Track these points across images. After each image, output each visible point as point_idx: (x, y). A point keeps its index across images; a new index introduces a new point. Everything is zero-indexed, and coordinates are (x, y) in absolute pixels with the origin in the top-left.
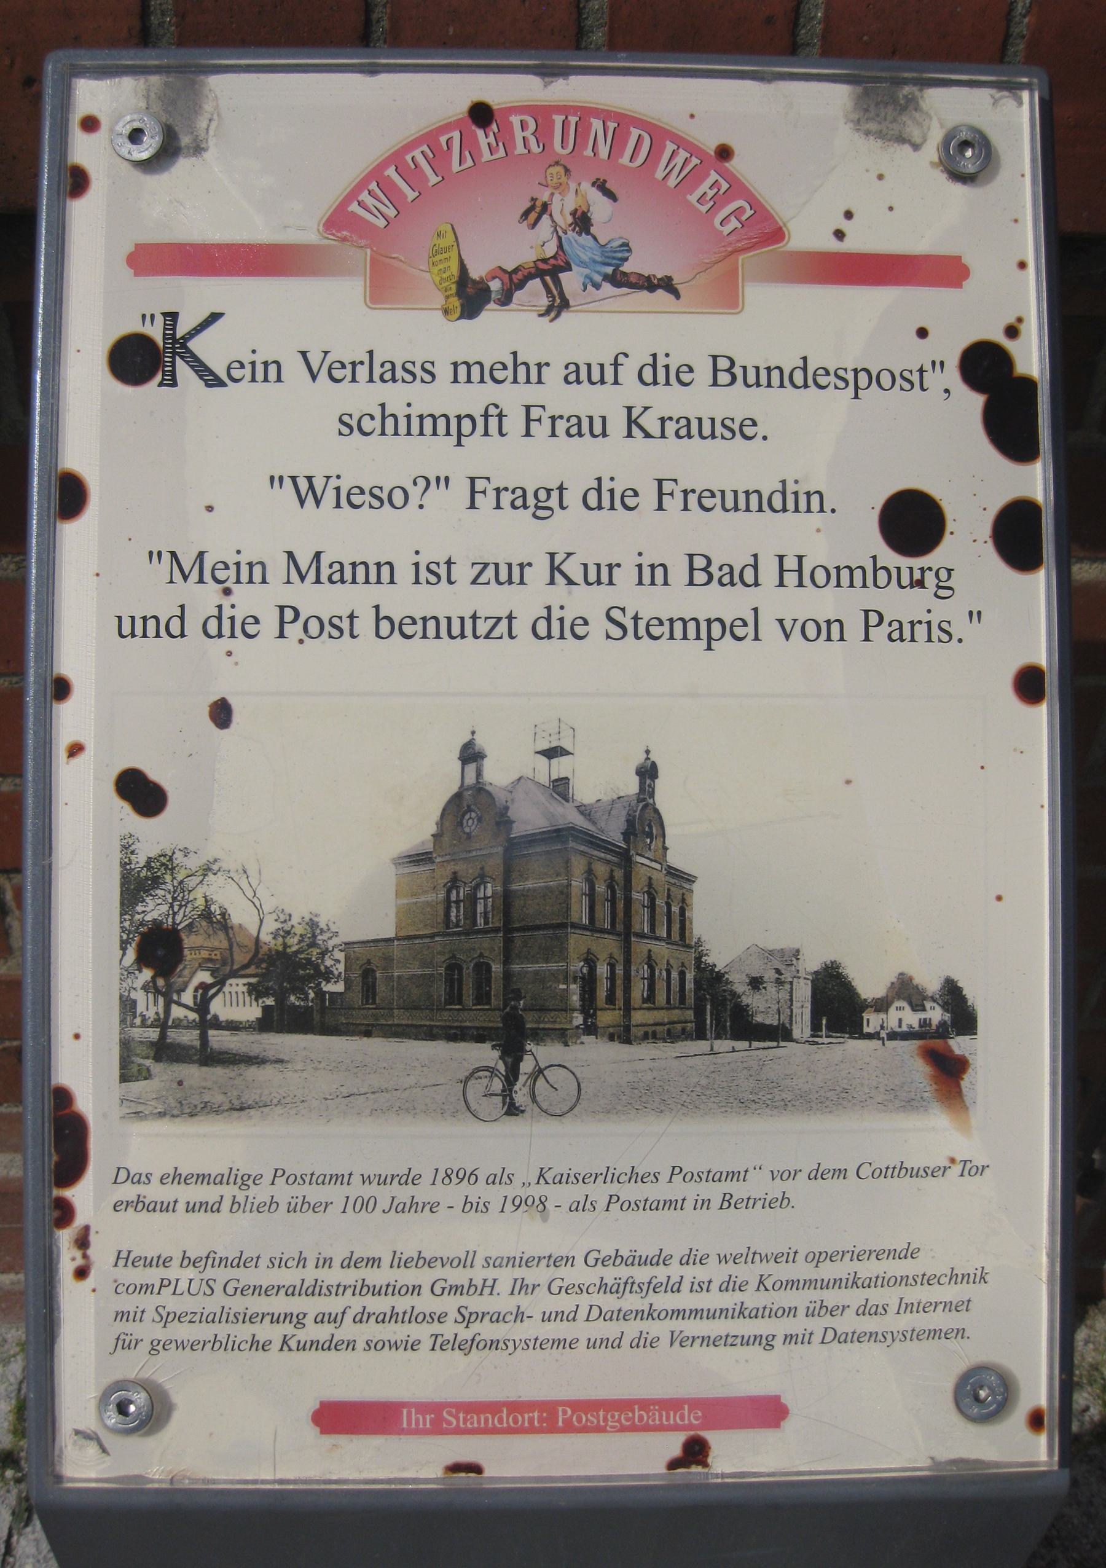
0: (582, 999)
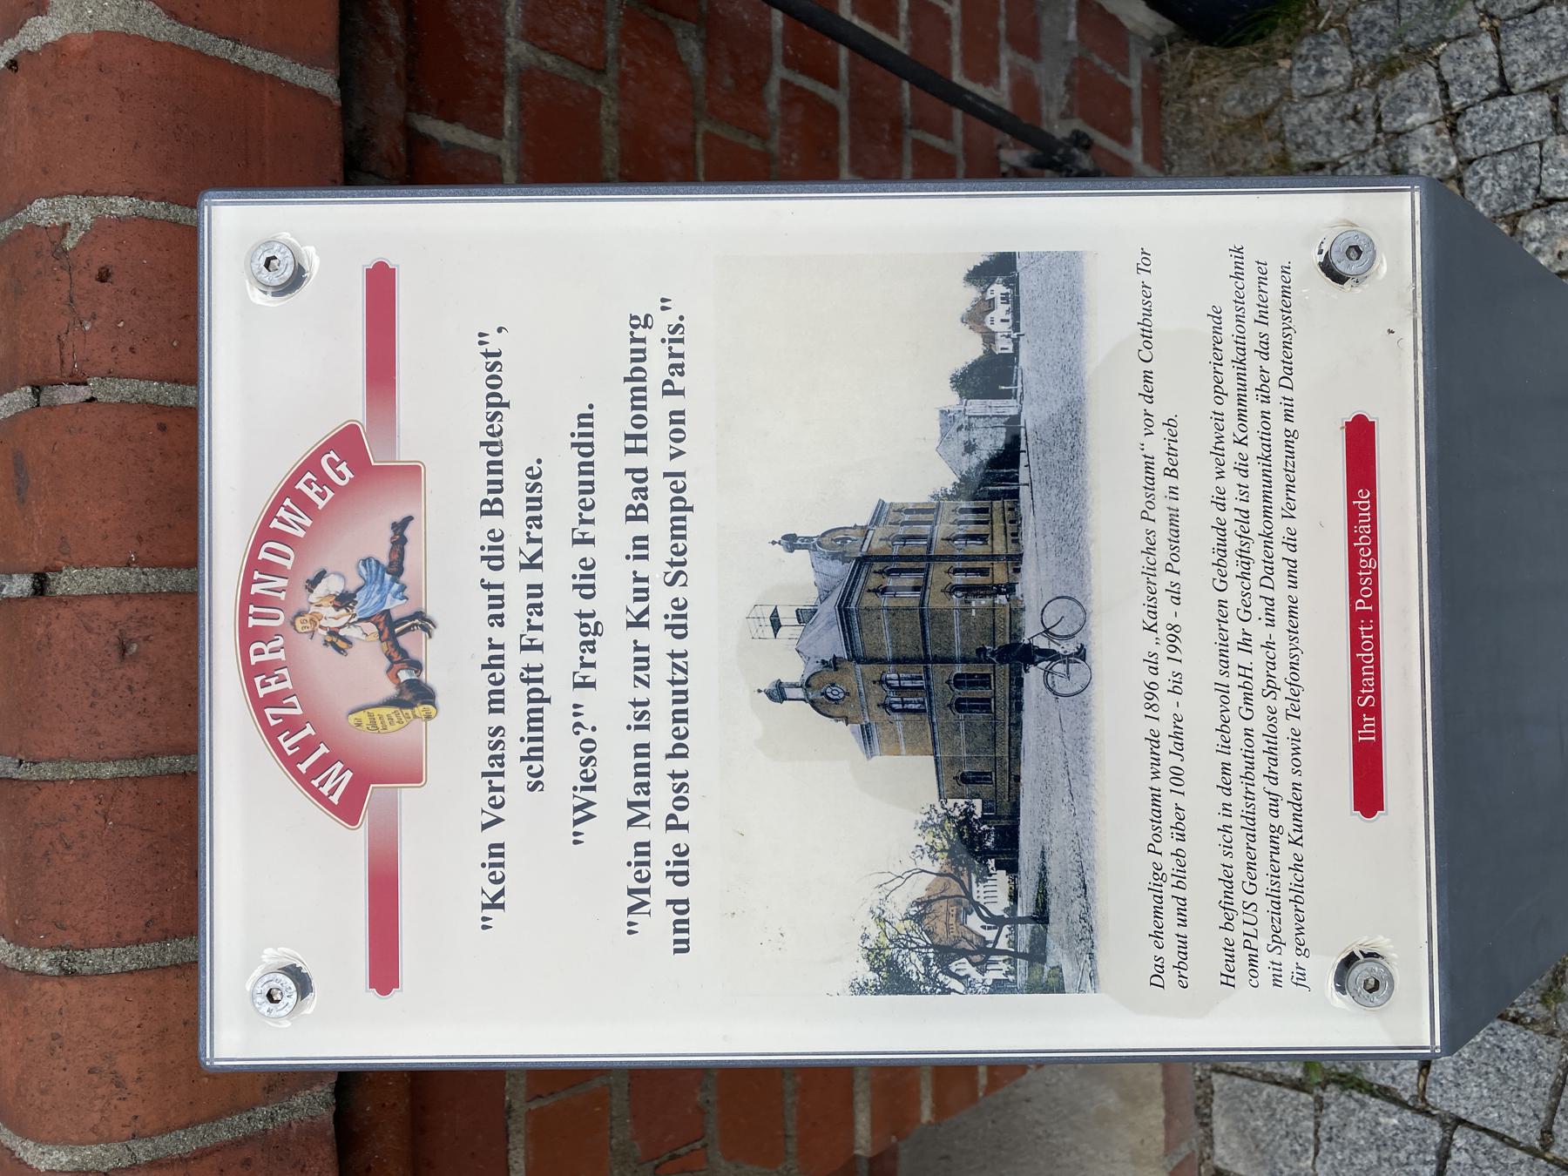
0: (983, 596)
